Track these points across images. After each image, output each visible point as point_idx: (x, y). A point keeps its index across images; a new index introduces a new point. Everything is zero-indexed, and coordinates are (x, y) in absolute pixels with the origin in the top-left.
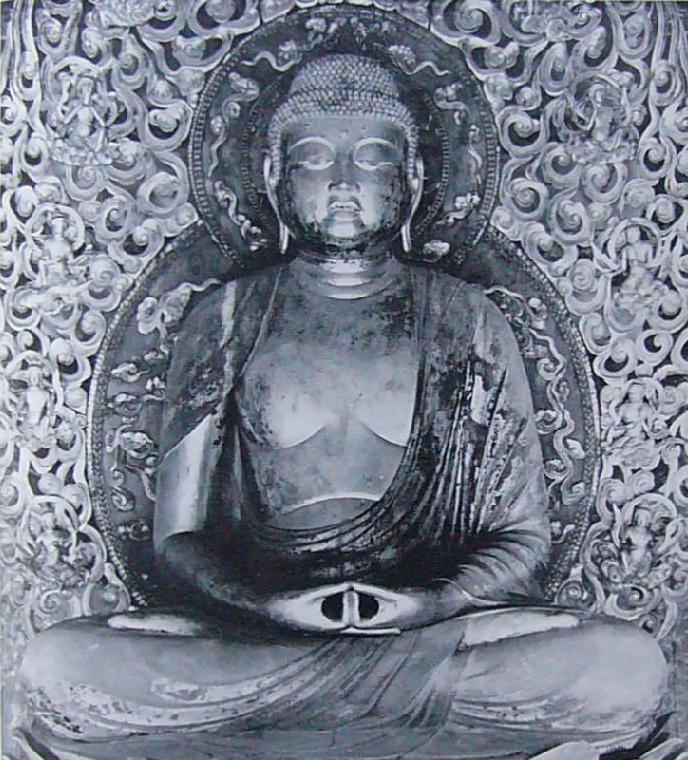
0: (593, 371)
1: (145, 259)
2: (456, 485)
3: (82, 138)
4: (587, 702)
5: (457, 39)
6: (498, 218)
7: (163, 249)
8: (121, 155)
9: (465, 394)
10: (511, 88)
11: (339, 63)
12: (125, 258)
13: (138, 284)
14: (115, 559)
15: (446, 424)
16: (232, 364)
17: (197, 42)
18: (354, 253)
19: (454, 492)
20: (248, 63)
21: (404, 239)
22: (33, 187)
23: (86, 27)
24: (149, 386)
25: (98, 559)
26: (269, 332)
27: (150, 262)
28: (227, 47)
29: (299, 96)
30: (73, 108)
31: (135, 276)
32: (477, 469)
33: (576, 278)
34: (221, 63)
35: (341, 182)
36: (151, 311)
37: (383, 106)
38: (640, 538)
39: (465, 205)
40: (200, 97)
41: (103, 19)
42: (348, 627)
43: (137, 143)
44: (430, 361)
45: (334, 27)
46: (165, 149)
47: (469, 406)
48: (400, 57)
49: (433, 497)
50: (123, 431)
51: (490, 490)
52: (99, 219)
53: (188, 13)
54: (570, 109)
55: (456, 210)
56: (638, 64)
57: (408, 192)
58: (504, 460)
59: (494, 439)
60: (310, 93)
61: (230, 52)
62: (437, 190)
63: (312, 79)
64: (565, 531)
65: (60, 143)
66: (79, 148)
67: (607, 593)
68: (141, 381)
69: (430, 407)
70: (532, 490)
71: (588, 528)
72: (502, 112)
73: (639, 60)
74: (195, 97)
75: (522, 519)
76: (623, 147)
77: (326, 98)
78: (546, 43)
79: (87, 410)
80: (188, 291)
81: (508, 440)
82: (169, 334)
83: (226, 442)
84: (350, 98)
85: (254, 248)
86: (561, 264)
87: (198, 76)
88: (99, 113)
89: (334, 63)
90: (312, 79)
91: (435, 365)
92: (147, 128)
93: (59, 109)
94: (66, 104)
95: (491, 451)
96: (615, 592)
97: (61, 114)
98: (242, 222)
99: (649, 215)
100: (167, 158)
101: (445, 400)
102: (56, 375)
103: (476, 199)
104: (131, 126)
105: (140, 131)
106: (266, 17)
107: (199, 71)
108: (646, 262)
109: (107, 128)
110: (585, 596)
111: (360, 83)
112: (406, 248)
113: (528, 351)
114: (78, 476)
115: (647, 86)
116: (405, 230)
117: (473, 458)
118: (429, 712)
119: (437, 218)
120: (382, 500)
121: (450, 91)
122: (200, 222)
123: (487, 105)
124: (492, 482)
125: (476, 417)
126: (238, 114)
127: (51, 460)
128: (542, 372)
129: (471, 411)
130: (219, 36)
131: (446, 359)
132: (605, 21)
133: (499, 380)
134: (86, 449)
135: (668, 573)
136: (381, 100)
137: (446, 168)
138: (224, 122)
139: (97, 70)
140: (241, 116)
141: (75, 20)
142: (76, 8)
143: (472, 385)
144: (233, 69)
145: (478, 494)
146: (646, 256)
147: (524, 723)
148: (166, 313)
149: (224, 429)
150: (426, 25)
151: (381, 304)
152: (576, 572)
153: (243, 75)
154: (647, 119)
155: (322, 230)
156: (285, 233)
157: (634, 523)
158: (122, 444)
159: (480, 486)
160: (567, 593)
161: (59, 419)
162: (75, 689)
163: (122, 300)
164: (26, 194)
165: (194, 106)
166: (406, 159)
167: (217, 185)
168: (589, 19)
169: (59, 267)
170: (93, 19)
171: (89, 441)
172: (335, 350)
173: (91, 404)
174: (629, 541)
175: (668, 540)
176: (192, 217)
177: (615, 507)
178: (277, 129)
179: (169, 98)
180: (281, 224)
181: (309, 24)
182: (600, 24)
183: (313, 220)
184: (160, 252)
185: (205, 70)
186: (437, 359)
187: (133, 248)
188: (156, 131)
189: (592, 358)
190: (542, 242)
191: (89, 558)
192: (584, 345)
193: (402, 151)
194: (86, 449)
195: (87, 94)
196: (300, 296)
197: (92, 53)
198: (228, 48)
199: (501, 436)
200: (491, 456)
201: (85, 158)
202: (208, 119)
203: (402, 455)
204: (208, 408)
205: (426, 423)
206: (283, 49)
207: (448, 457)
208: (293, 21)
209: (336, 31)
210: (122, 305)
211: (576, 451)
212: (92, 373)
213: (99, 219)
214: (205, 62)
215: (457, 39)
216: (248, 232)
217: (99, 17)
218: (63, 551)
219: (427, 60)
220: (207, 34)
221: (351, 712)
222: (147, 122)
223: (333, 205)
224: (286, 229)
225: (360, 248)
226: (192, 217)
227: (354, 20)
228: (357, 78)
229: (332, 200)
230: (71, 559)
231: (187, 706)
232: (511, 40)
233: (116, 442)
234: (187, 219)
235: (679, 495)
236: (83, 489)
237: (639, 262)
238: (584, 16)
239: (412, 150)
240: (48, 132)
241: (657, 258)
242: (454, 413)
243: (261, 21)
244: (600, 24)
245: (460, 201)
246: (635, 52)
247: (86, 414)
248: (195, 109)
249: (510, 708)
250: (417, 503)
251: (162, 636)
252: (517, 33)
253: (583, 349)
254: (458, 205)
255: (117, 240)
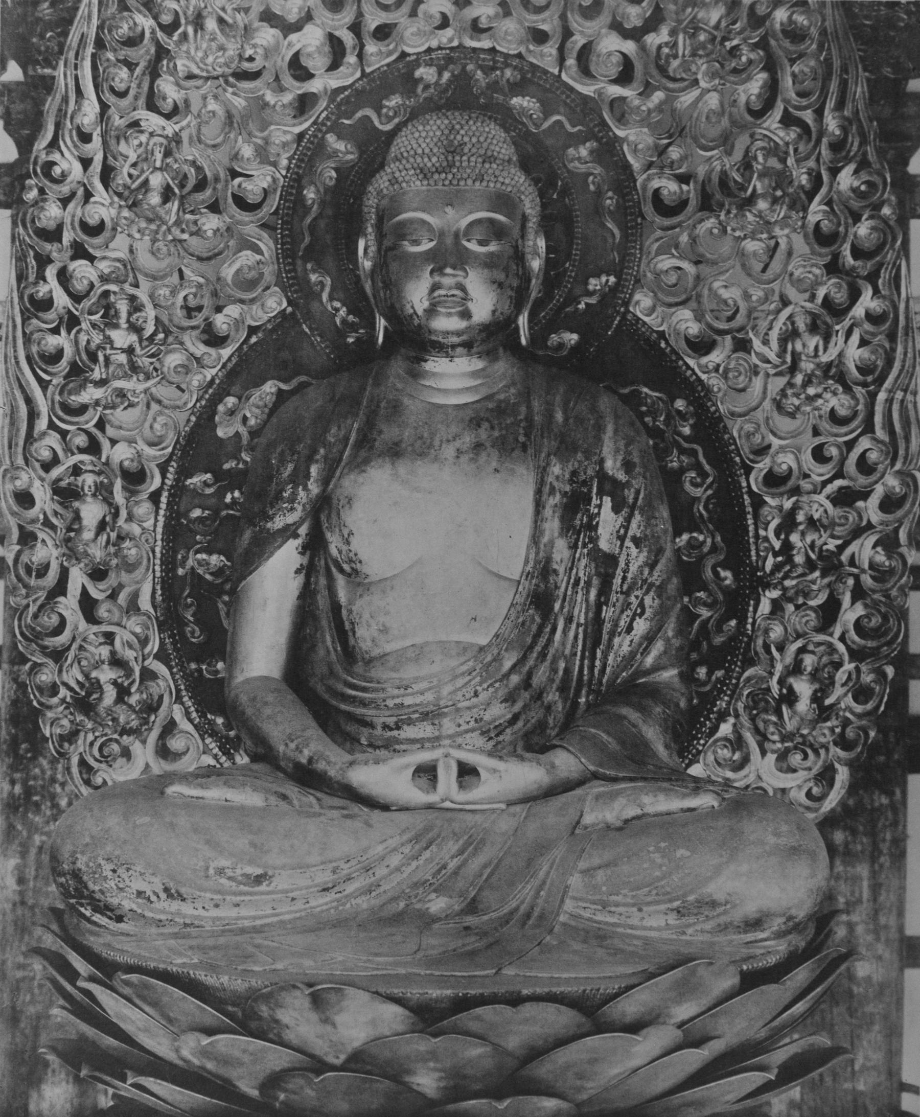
0: (749, 486)
1: (226, 352)
2: (579, 625)
3: (153, 208)
4: (728, 906)
5: (593, 88)
6: (638, 303)
7: (246, 341)
8: (199, 229)
9: (591, 517)
10: (656, 146)
11: (446, 122)
12: (200, 349)
13: (217, 381)
14: (186, 699)
15: (566, 554)
16: (316, 481)
17: (288, 98)
18: (459, 350)
19: (576, 637)
20: (346, 122)
21: (522, 333)
22: (92, 263)
23: (160, 76)
24: (228, 498)
25: (166, 699)
26: (359, 445)
27: (232, 355)
28: (323, 104)
29: (397, 164)
30: (143, 171)
31: (214, 371)
32: (605, 608)
33: (730, 375)
34: (315, 123)
35: (445, 267)
36: (232, 413)
37: (497, 173)
38: (803, 688)
39: (598, 287)
40: (290, 163)
41: (179, 67)
42: (443, 801)
43: (217, 216)
44: (550, 479)
45: (446, 75)
46: (249, 225)
47: (596, 531)
48: (523, 111)
49: (550, 641)
50: (197, 552)
51: (620, 634)
52: (173, 304)
53: (279, 62)
54: (725, 172)
55: (591, 294)
56: (808, 116)
57: (526, 277)
58: (637, 597)
59: (625, 571)
60: (427, 151)
61: (326, 109)
62: (566, 270)
63: (413, 142)
64: (714, 678)
65: (126, 213)
66: (150, 221)
67: (763, 753)
68: (220, 493)
69: (547, 533)
70: (670, 634)
71: (741, 674)
72: (645, 176)
73: (809, 111)
74: (284, 162)
75: (656, 668)
76: (790, 217)
77: (429, 165)
78: (699, 91)
79: (155, 526)
80: (274, 390)
81: (642, 574)
82: (252, 439)
83: (308, 571)
84: (457, 164)
85: (350, 340)
86: (715, 357)
87: (289, 137)
88: (173, 179)
89: (439, 122)
90: (413, 142)
91: (556, 484)
92: (230, 200)
93: (125, 170)
94: (134, 165)
95: (621, 586)
96: (773, 752)
97: (128, 179)
98: (337, 310)
99: (819, 300)
100: (252, 233)
101: (567, 527)
102: (118, 484)
103: (612, 279)
104: (212, 196)
105: (221, 202)
106: (369, 66)
107: (289, 132)
108: (816, 355)
109: (182, 198)
110: (737, 756)
111: (469, 146)
112: (524, 341)
113: (672, 461)
114: (145, 603)
115: (818, 142)
116: (523, 320)
117: (599, 595)
118: (536, 914)
119: (566, 304)
120: (489, 645)
121: (584, 152)
122: (290, 309)
123: (627, 166)
124: (622, 623)
125: (604, 545)
126: (333, 183)
127: (112, 580)
128: (688, 487)
129: (598, 538)
130: (314, 90)
131: (567, 476)
132: (771, 66)
133: (631, 501)
134: (154, 571)
135: (838, 730)
136: (494, 166)
137: (577, 244)
138: (318, 191)
139: (170, 128)
140: (336, 186)
141: (147, 68)
142: (147, 52)
143: (599, 506)
144: (330, 130)
145: (605, 637)
146: (816, 348)
147: (651, 929)
148: (248, 415)
149: (308, 553)
150: (556, 71)
151: (492, 410)
152: (725, 729)
153: (340, 137)
154: (817, 182)
155: (423, 322)
156: (381, 323)
157: (796, 669)
158: (196, 566)
159: (607, 627)
160: (715, 752)
161: (121, 538)
162: (120, 871)
163: (197, 401)
164: (82, 271)
165: (284, 173)
166: (523, 237)
167: (309, 266)
168: (750, 62)
169: (122, 358)
170: (168, 67)
171: (158, 562)
172: (436, 465)
173: (161, 519)
174: (791, 689)
175: (838, 691)
176: (280, 304)
177: (773, 650)
178: (371, 202)
179: (255, 164)
180: (377, 316)
181: (418, 73)
182: (763, 69)
183: (411, 311)
184: (243, 344)
185: (297, 130)
186: (557, 478)
187: (214, 340)
188: (241, 202)
189: (748, 470)
190: (691, 331)
191: (156, 698)
192: (740, 455)
193: (518, 227)
194: (154, 571)
195: (159, 156)
196: (396, 401)
197: (167, 106)
198: (325, 104)
199: (633, 568)
200: (622, 593)
201: (157, 232)
202: (300, 189)
203: (514, 590)
204: (289, 532)
205: (542, 554)
206: (387, 104)
207: (569, 593)
208: (399, 70)
209: (449, 80)
210: (198, 405)
211: (728, 582)
212: (163, 483)
213: (173, 304)
214: (296, 121)
215: (593, 88)
216: (344, 321)
217: (175, 65)
218: (123, 693)
219: (559, 113)
220: (299, 88)
221: (443, 905)
222: (230, 191)
223: (436, 294)
224: (383, 321)
225: (468, 345)
226: (280, 304)
227: (470, 67)
228: (466, 139)
229: (435, 287)
230: (133, 699)
231: (251, 894)
232: (657, 88)
233: (190, 562)
234: (274, 305)
235: (853, 635)
236: (149, 618)
237: (807, 356)
238: (744, 59)
239: (532, 224)
240: (111, 198)
241: (828, 352)
242: (577, 540)
243: (363, 71)
244: (763, 69)
245: (594, 284)
246: (804, 102)
247: (154, 531)
248: (285, 177)
249: (635, 909)
250: (531, 648)
251: (227, 810)
252: (664, 81)
253: (737, 459)
254: (591, 288)
255: (193, 328)
